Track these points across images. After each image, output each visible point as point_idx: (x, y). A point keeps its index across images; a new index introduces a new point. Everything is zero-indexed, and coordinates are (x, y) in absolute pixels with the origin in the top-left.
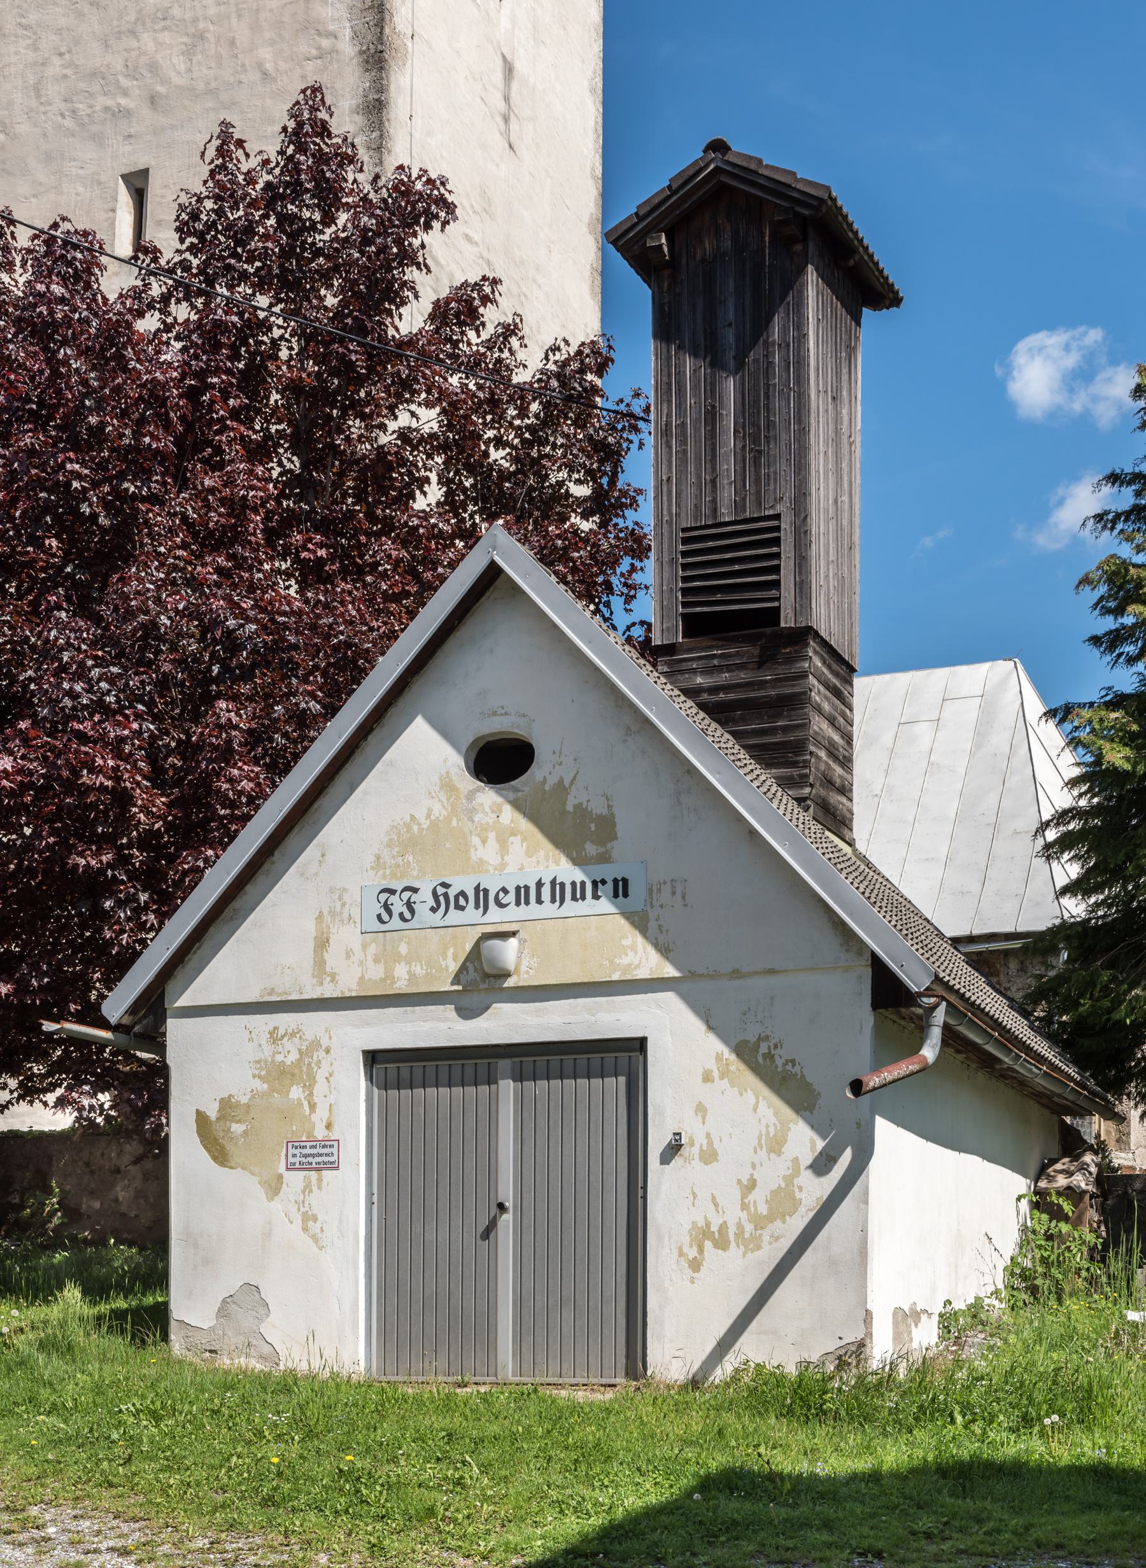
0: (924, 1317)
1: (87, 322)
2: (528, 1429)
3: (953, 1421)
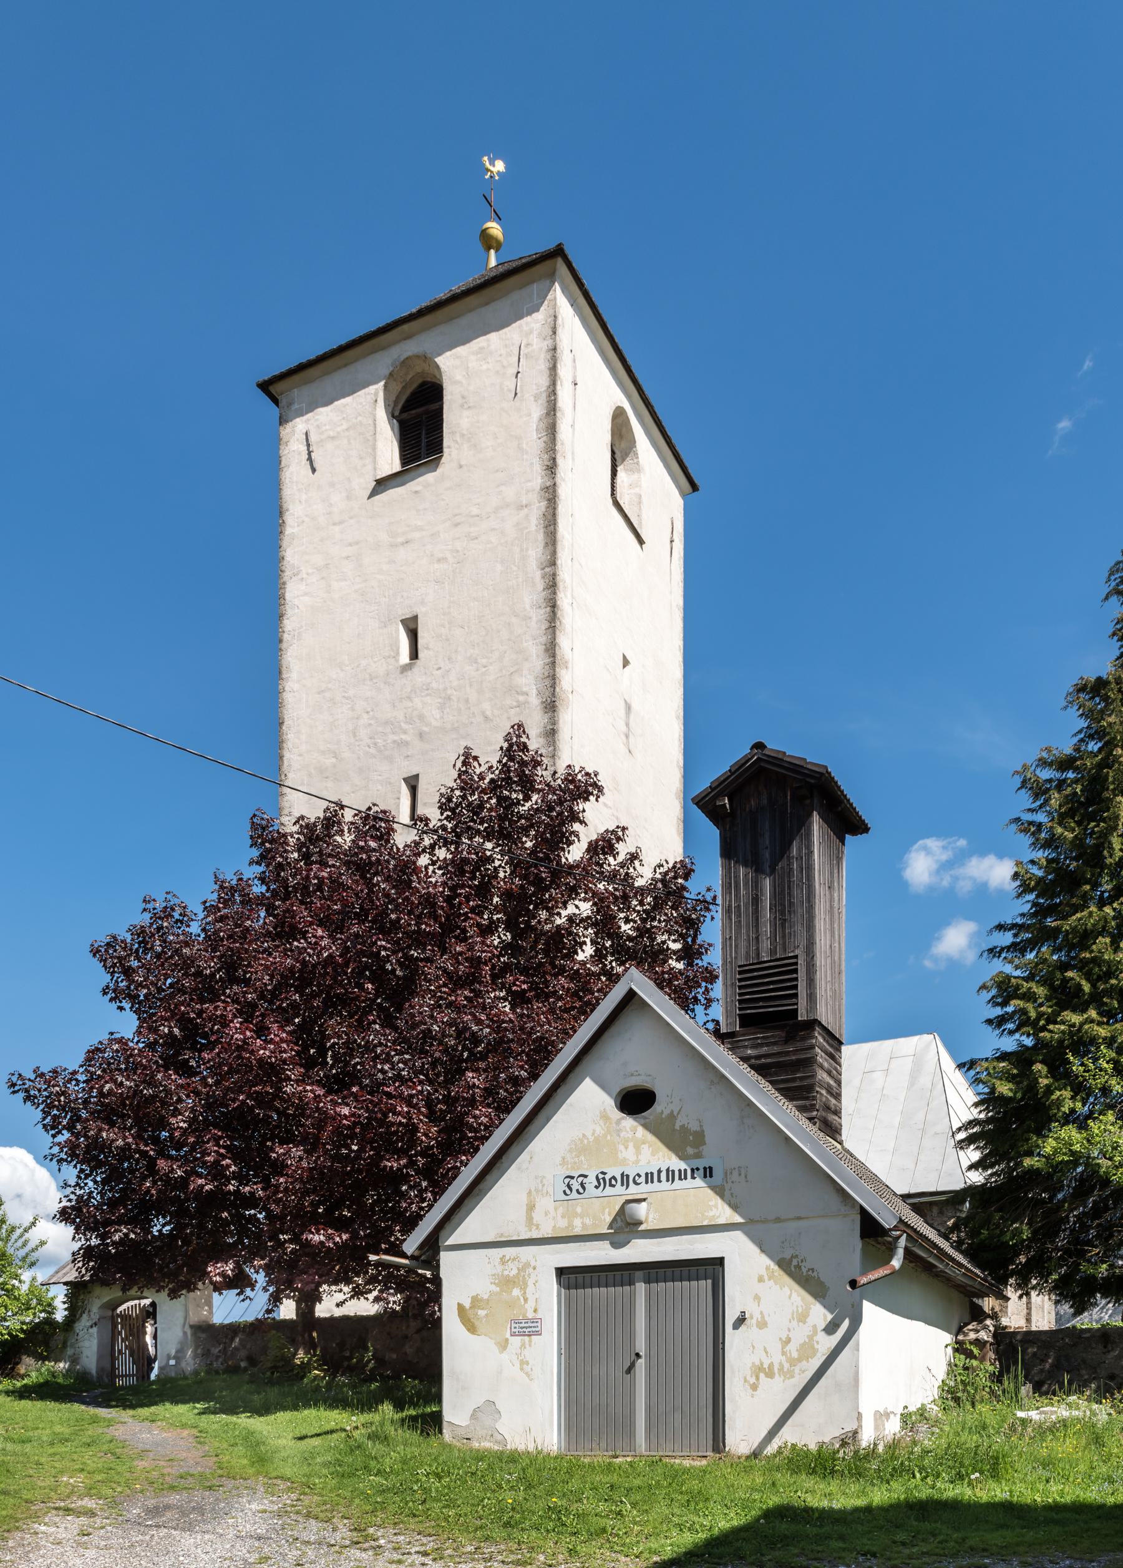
0: (892, 1416)
1: (388, 861)
2: (658, 1482)
3: (914, 1477)
